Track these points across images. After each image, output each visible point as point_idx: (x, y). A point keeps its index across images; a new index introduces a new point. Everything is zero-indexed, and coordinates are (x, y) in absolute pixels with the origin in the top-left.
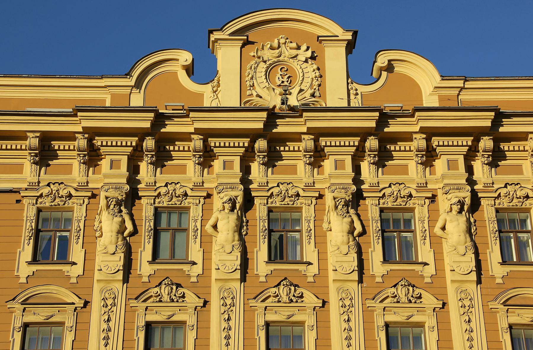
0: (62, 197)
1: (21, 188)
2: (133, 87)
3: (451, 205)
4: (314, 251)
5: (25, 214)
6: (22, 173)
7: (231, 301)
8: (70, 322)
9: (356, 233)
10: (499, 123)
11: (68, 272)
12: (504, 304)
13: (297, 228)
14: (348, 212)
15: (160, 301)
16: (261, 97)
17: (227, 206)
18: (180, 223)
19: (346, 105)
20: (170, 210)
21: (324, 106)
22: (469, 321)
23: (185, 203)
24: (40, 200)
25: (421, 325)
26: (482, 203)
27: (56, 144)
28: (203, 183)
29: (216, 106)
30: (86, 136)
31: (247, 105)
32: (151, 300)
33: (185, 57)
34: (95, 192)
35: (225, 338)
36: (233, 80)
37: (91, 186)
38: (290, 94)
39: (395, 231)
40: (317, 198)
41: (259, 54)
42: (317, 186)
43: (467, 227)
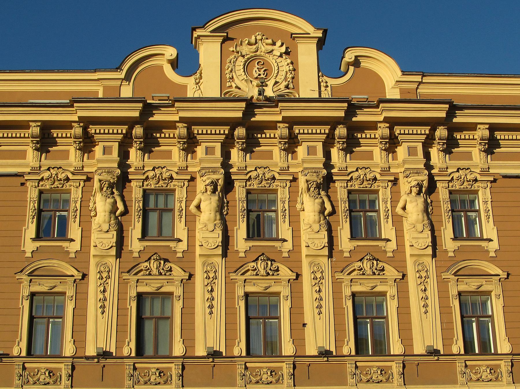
0: (61, 180)
1: (25, 173)
2: (123, 79)
3: (411, 187)
4: (288, 229)
5: (29, 196)
6: (25, 159)
7: (213, 274)
8: (70, 292)
9: (326, 213)
10: (452, 115)
11: (67, 248)
12: (455, 274)
13: (273, 208)
14: (319, 194)
15: (150, 274)
16: (240, 89)
17: (209, 188)
18: (166, 204)
19: (316, 96)
20: (157, 192)
21: (297, 96)
22: (425, 290)
23: (171, 186)
24: (41, 183)
25: (383, 294)
26: (438, 186)
27: (55, 133)
28: (187, 167)
29: (198, 96)
30: (82, 124)
31: (227, 96)
32: (142, 273)
33: (171, 52)
34: (90, 175)
35: (209, 307)
36: (213, 73)
37: (86, 170)
38: (267, 86)
39: (362, 212)
40: (291, 181)
41: (238, 49)
42: (291, 170)
43: (424, 207)
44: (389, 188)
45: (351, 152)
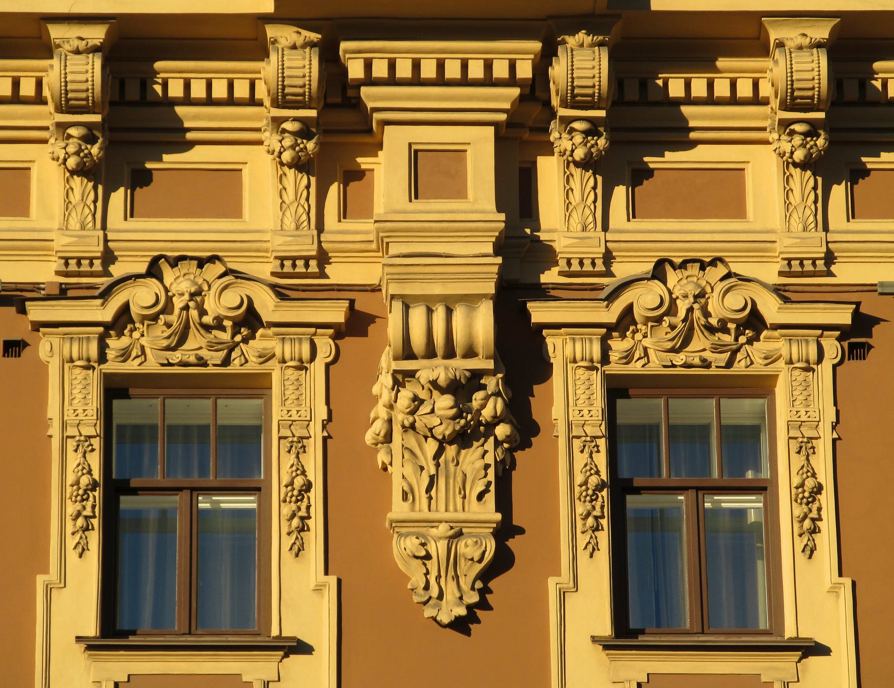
1: (35, 287)
4: (318, 589)
27: (173, 76)
34: (364, 304)
44: (318, 369)
45: (639, 175)
